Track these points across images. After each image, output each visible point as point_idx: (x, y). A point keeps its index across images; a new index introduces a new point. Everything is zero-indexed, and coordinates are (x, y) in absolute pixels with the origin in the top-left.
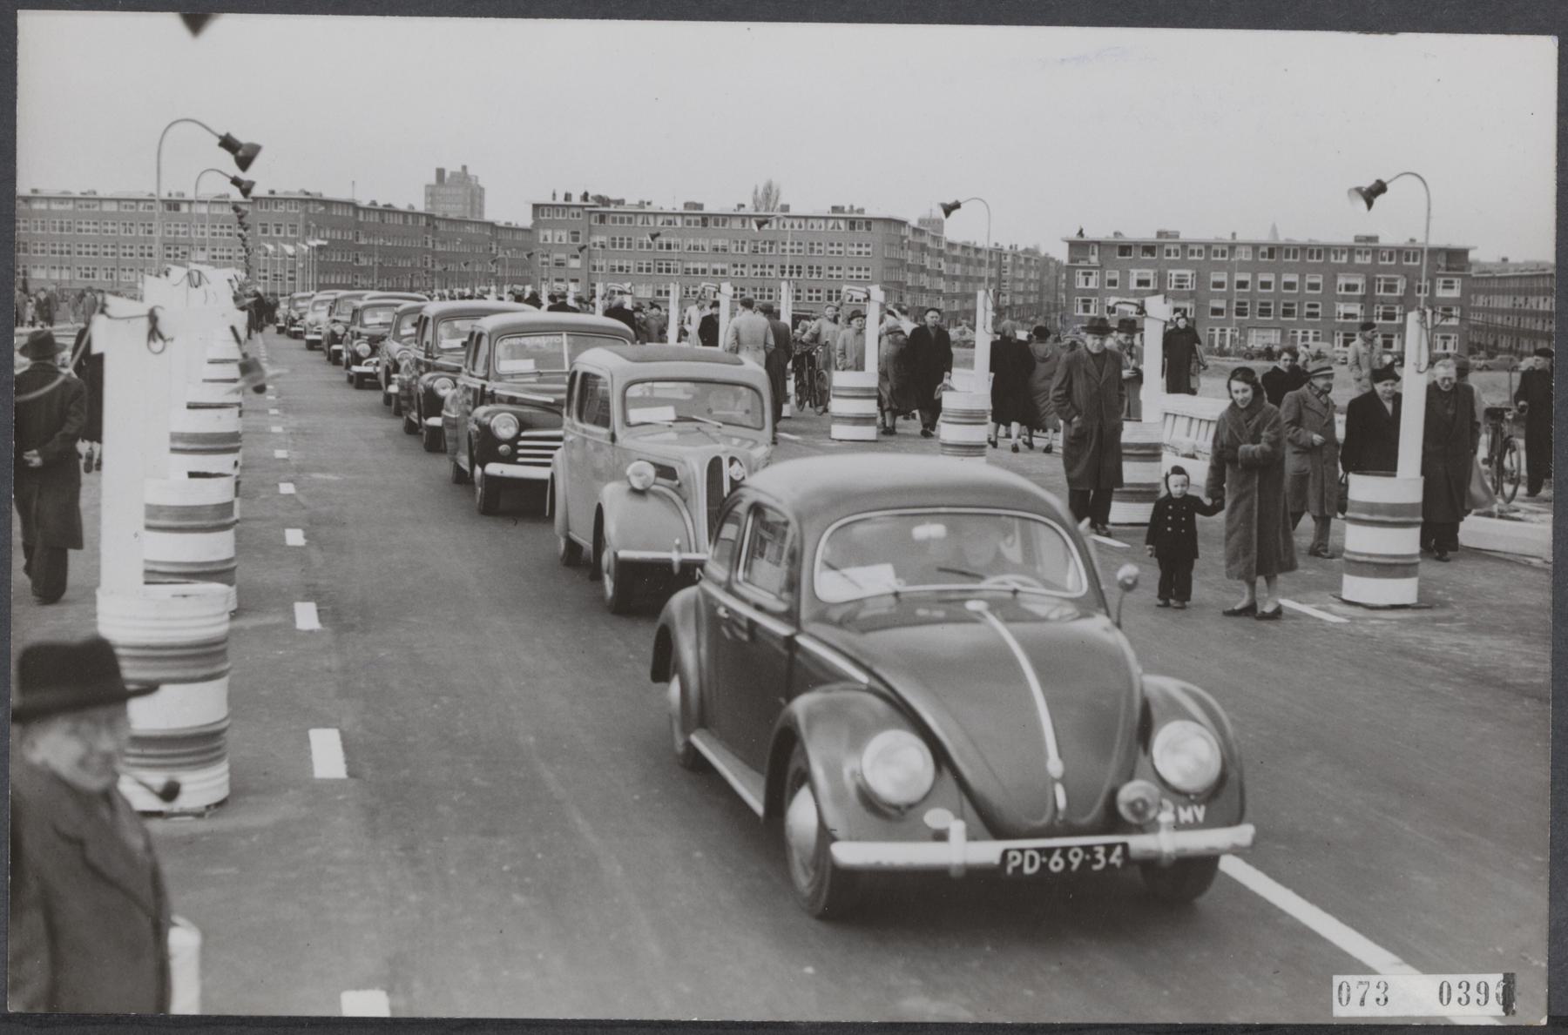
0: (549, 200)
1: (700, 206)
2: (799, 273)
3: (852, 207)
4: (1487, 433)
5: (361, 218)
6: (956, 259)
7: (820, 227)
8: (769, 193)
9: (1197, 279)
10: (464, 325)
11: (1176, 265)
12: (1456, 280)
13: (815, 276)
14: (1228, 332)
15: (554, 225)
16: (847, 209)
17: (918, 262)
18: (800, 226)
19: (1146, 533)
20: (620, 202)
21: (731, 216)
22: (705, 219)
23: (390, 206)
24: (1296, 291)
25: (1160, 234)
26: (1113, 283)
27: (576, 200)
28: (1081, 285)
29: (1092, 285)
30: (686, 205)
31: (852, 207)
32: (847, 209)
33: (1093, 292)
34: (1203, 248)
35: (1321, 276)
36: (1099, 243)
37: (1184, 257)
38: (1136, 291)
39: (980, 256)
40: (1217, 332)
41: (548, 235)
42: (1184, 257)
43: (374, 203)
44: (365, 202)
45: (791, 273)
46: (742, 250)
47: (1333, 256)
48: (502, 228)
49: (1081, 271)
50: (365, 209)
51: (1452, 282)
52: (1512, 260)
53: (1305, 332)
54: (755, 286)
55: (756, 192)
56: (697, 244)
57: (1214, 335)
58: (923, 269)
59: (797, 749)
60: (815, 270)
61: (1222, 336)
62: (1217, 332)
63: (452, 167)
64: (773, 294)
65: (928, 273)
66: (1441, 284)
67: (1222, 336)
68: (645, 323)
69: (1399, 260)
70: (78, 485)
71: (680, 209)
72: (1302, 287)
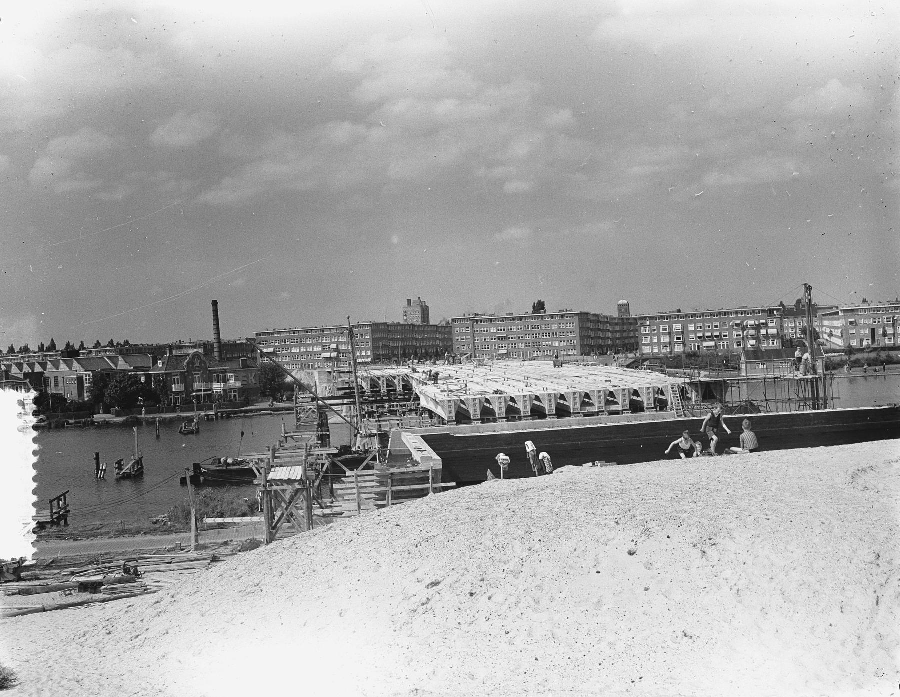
2: (549, 336)
5: (390, 329)
10: (594, 377)
12: (774, 319)
13: (548, 337)
17: (597, 327)
19: (36, 369)
23: (399, 323)
24: (719, 328)
26: (717, 326)
28: (644, 332)
29: (647, 332)
33: (648, 334)
35: (681, 324)
38: (662, 333)
40: (693, 345)
44: (390, 322)
45: (546, 336)
46: (528, 328)
49: (643, 327)
51: (773, 320)
54: (534, 341)
55: (39, 346)
58: (599, 330)
60: (555, 334)
62: (693, 345)
64: (541, 344)
65: (602, 331)
66: (770, 321)
67: (695, 346)
68: (843, 367)
72: (712, 327)
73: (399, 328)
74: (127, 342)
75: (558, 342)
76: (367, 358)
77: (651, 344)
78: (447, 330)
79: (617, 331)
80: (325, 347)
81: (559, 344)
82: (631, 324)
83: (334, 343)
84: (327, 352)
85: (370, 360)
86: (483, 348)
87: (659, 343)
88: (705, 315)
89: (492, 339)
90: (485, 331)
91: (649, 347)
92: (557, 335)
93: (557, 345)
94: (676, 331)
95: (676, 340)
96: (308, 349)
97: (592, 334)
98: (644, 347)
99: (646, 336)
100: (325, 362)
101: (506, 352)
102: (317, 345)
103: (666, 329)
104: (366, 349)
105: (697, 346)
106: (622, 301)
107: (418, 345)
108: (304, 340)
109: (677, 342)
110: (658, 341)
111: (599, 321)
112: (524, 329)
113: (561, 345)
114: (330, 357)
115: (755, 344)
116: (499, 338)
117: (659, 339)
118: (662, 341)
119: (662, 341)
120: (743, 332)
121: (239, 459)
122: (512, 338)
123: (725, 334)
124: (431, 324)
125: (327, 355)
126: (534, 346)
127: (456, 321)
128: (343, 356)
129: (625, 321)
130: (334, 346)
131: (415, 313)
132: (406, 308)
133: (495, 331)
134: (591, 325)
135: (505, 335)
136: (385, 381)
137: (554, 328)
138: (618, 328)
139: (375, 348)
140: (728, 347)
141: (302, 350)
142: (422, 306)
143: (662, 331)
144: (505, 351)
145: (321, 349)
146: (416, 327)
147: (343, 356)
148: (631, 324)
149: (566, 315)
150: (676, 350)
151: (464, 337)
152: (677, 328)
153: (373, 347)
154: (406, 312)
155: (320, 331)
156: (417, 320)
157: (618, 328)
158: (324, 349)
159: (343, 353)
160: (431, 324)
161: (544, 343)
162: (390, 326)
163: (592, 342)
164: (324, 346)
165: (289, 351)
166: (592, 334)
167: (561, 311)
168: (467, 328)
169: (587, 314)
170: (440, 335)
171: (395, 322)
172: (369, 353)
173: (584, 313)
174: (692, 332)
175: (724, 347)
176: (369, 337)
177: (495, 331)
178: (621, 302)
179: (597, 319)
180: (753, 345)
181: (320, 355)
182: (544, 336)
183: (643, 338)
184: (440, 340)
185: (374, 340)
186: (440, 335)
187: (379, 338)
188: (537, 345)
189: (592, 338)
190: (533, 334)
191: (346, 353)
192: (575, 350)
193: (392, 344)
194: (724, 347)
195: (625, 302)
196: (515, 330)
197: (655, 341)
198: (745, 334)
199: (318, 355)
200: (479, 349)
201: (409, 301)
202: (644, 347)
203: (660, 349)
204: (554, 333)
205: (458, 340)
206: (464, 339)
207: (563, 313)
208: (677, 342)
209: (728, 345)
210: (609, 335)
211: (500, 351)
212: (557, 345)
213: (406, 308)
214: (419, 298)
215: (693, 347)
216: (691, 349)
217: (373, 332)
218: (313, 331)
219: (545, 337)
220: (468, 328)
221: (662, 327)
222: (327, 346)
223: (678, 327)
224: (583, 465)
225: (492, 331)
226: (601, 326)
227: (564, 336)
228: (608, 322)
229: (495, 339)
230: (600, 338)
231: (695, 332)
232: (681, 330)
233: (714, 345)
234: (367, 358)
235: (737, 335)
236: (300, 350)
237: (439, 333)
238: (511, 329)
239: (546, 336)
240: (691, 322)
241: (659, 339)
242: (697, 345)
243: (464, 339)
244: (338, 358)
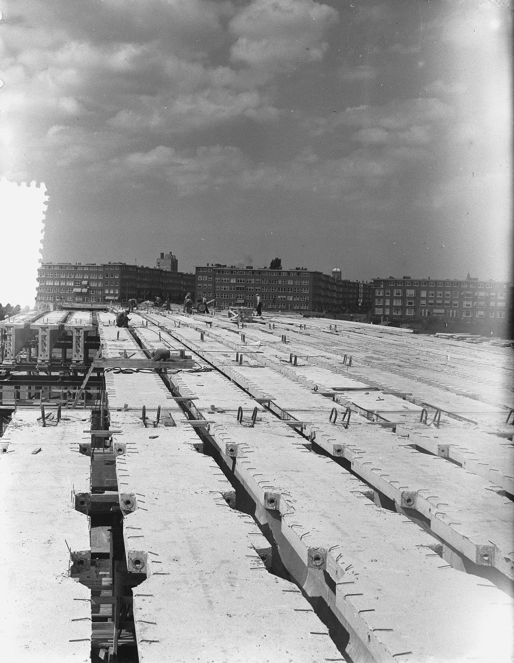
0: (206, 266)
1: (252, 268)
3: (302, 268)
4: (61, 374)
6: (341, 286)
7: (285, 275)
8: (44, 212)
9: (416, 293)
11: (409, 288)
13: (283, 291)
14: (427, 310)
15: (203, 274)
16: (301, 269)
18: (285, 275)
20: (225, 266)
21: (84, 266)
22: (253, 272)
23: (148, 267)
25: (404, 278)
26: (388, 294)
27: (210, 266)
29: (381, 295)
30: (247, 267)
31: (302, 268)
32: (301, 269)
34: (418, 282)
35: (414, 290)
36: (383, 280)
37: (396, 285)
39: (350, 285)
41: (200, 278)
42: (396, 285)
43: (142, 266)
45: (282, 290)
46: (266, 282)
47: (462, 286)
48: (185, 275)
50: (140, 268)
52: (37, 276)
53: (453, 311)
56: (250, 280)
57: (422, 312)
58: (328, 289)
59: (405, 514)
61: (425, 312)
63: (279, 259)
67: (425, 312)
69: (404, 284)
70: (12, 385)
71: (245, 268)
73: (147, 272)
74: (276, 264)
75: (292, 297)
76: (115, 297)
77: (384, 307)
78: (190, 279)
79: (340, 293)
80: (77, 283)
81: (293, 299)
82: (350, 287)
83: (85, 280)
84: (79, 287)
85: (117, 298)
86: (222, 297)
87: (391, 307)
88: (414, 282)
89: (232, 289)
90: (225, 281)
91: (381, 309)
92: (291, 291)
93: (291, 299)
94: (408, 296)
95: (408, 305)
96: (68, 284)
97: (323, 293)
98: (376, 309)
99: (379, 298)
100: (76, 297)
101: (243, 302)
102: (69, 280)
103: (399, 294)
104: (114, 288)
105: (455, 314)
106: (336, 269)
107: (164, 289)
108: (59, 275)
109: (408, 307)
110: (390, 304)
111: (328, 282)
112: (262, 282)
113: (295, 300)
114: (81, 292)
115: (483, 314)
116: (238, 288)
117: (391, 303)
118: (394, 304)
119: (394, 304)
120: (473, 303)
121: (46, 348)
122: (250, 290)
123: (455, 303)
124: (178, 271)
125: (79, 290)
126: (270, 298)
127: (199, 269)
128: (93, 292)
129: (347, 284)
130: (85, 283)
131: (166, 264)
132: (159, 259)
133: (235, 282)
134: (322, 285)
135: (244, 287)
136: (82, 339)
137: (289, 284)
138: (341, 290)
139: (122, 288)
140: (456, 315)
141: (56, 284)
142: (172, 259)
143: (395, 295)
144: (243, 301)
145: (73, 285)
146: (163, 273)
147: (93, 292)
148: (350, 287)
149: (303, 273)
150: (407, 314)
151: (206, 285)
152: (410, 294)
153: (121, 287)
154: (159, 263)
155: (73, 267)
156: (167, 267)
157: (341, 290)
158: (76, 284)
159: (93, 290)
160: (178, 271)
161: (279, 297)
162: (139, 269)
163: (322, 300)
164: (76, 282)
165: (44, 284)
166: (323, 293)
167: (297, 269)
168: (209, 277)
169: (320, 273)
170: (184, 282)
171: (145, 267)
172: (117, 292)
173: (317, 273)
174: (423, 298)
175: (453, 315)
176: (118, 278)
177: (235, 282)
178: (335, 270)
179: (327, 279)
180: (481, 316)
181: (72, 289)
182: (279, 290)
183: (377, 300)
184: (184, 286)
185: (122, 281)
186: (184, 282)
187: (127, 279)
188: (272, 298)
189: (322, 296)
190: (270, 288)
191: (96, 290)
192: (307, 305)
193: (138, 286)
194: (453, 315)
195: (338, 270)
196: (253, 282)
197: (388, 303)
198: (474, 305)
199: (70, 289)
200: (218, 297)
201: (162, 254)
202: (376, 309)
203: (391, 312)
204: (289, 289)
205: (200, 287)
206: (206, 287)
207: (299, 271)
208: (408, 307)
209: (457, 313)
210: (335, 295)
211: (238, 301)
212: (291, 299)
213: (159, 259)
214: (171, 253)
215: (455, 314)
216: (421, 314)
217: (122, 275)
218: (67, 267)
219: (280, 291)
220: (211, 277)
221: (395, 291)
222: (78, 282)
223: (411, 292)
224: (416, 524)
225: (232, 282)
226: (330, 287)
227: (275, 291)
228: (335, 284)
229: (234, 289)
230: (328, 296)
231: (427, 299)
232: (413, 296)
233: (444, 312)
234: (115, 297)
235: (467, 305)
236: (109, 292)
237: (184, 281)
238: (250, 282)
239: (282, 290)
240: (424, 289)
241: (391, 303)
242: (427, 310)
243: (206, 287)
244: (87, 294)
